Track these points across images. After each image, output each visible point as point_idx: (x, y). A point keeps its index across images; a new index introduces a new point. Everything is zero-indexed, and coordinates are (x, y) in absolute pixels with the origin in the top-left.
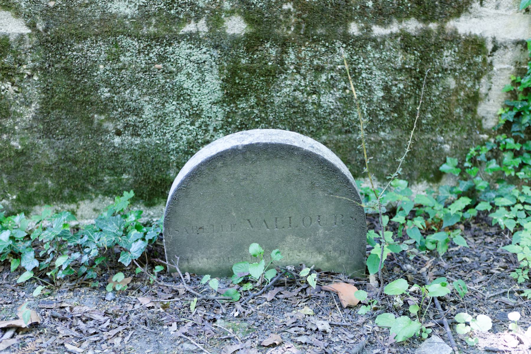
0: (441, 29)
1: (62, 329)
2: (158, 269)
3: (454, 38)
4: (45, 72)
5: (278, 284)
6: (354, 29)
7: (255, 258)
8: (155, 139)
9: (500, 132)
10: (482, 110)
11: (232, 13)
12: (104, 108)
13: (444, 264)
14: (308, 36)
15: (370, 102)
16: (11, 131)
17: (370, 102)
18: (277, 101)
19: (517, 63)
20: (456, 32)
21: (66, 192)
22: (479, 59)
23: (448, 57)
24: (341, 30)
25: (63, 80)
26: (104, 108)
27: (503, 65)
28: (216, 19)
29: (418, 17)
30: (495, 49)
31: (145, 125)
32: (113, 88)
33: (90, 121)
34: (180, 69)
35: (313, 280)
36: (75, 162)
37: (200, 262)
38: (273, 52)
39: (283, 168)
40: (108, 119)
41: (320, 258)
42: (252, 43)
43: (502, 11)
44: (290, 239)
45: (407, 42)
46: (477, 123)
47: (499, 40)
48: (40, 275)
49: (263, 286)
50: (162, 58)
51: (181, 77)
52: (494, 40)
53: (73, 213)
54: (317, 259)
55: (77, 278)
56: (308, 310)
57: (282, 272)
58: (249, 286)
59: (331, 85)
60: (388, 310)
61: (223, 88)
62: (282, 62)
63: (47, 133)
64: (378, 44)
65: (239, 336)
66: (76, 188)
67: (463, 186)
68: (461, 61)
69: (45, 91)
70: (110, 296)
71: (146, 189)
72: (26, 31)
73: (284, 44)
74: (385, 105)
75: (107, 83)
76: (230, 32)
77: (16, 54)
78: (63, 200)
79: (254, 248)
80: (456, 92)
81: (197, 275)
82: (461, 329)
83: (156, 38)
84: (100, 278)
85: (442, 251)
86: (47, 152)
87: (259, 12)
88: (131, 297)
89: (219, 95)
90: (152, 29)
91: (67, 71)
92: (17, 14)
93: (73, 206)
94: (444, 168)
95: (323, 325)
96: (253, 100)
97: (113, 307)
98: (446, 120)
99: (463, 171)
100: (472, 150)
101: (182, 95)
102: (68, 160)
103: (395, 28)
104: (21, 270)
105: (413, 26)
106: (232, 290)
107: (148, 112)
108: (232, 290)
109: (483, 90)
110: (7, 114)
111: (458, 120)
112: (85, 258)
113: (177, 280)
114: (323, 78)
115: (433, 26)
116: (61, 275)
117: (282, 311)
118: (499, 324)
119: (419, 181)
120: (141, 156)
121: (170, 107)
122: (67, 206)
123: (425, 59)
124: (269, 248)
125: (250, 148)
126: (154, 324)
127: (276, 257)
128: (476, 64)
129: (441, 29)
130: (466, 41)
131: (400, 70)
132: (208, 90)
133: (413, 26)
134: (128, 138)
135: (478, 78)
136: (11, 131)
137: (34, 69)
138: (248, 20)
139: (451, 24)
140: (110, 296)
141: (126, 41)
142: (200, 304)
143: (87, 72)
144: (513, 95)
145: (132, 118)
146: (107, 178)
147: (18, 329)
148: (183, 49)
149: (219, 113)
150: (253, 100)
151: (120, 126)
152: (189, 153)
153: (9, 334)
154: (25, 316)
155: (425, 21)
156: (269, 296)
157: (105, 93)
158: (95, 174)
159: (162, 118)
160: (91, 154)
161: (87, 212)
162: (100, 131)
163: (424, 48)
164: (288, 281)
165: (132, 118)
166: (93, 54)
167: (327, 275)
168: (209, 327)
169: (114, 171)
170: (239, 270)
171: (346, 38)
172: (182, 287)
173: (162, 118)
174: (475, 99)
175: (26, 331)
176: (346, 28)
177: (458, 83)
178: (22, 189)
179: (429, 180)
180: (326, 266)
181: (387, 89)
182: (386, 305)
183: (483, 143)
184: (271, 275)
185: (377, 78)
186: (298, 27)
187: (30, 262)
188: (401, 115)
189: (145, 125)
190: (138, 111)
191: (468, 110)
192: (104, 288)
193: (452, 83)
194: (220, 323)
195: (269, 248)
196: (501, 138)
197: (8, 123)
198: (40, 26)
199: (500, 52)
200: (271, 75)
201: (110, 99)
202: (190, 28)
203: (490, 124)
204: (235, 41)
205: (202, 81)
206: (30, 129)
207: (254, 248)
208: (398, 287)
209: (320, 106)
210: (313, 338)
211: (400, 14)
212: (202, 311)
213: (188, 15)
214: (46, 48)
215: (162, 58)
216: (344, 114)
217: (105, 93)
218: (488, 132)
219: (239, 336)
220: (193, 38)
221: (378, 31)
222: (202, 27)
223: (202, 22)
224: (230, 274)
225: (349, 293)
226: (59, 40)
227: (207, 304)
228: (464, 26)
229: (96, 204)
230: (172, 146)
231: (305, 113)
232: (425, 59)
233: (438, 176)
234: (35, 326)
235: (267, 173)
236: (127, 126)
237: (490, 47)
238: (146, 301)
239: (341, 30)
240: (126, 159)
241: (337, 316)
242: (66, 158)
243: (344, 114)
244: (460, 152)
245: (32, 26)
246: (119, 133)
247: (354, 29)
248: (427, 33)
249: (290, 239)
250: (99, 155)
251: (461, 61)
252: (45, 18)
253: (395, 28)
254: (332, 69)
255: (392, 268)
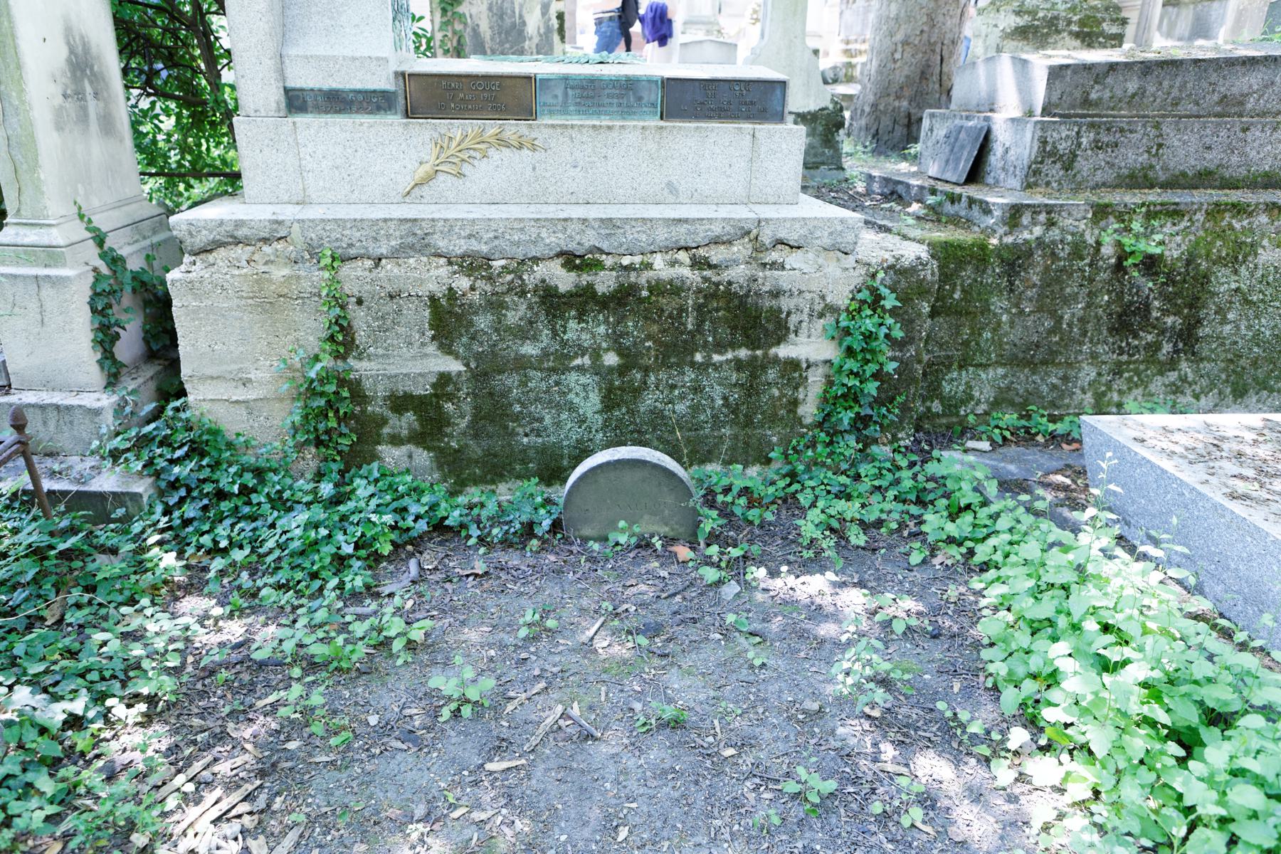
0: (766, 355)
1: (503, 575)
2: (559, 536)
3: (776, 360)
4: (475, 396)
5: (638, 546)
6: (698, 357)
7: (623, 531)
8: (553, 439)
9: (816, 426)
10: (801, 411)
11: (608, 350)
12: (517, 418)
13: (757, 532)
14: (663, 363)
15: (713, 408)
16: (451, 436)
17: (713, 408)
18: (642, 409)
19: (827, 376)
20: (777, 356)
21: (489, 477)
22: (797, 375)
23: (772, 374)
24: (689, 358)
25: (489, 401)
26: (517, 418)
27: (816, 380)
28: (596, 354)
29: (747, 347)
30: (808, 367)
31: (545, 430)
32: (523, 405)
33: (506, 427)
34: (570, 390)
35: (658, 545)
36: (495, 456)
37: (587, 531)
38: (638, 376)
39: (639, 474)
40: (519, 425)
41: (667, 529)
42: (622, 370)
43: (813, 339)
44: (646, 517)
45: (739, 365)
46: (799, 421)
47: (812, 360)
48: (481, 540)
49: (628, 549)
50: (557, 384)
51: (571, 396)
52: (807, 361)
53: (494, 492)
54: (664, 530)
55: (506, 543)
56: (657, 564)
57: (641, 538)
58: (619, 548)
59: (682, 397)
60: (707, 564)
61: (602, 402)
62: (645, 383)
63: (476, 436)
64: (717, 367)
65: (611, 580)
66: (496, 474)
67: (787, 468)
68: (783, 377)
69: (475, 408)
70: (529, 554)
71: (546, 474)
72: (463, 368)
73: (646, 370)
74: (725, 410)
75: (519, 401)
76: (606, 363)
77: (455, 384)
78: (487, 483)
79: (622, 524)
80: (780, 398)
81: (585, 540)
82: (749, 577)
83: (553, 370)
84: (521, 543)
85: (757, 522)
86: (476, 449)
87: (628, 348)
88: (543, 554)
89: (599, 407)
90: (551, 364)
91: (491, 394)
92: (457, 357)
93: (493, 487)
94: (772, 455)
95: (664, 573)
96: (624, 410)
97: (532, 561)
98: (773, 419)
99: (787, 456)
100: (794, 442)
101: (572, 408)
102: (490, 454)
103: (729, 356)
104: (469, 537)
105: (743, 353)
106: (608, 551)
107: (548, 420)
108: (608, 551)
109: (801, 396)
110: (449, 424)
111: (782, 418)
112: (512, 530)
113: (572, 544)
114: (676, 392)
115: (759, 353)
116: (496, 540)
117: (639, 565)
118: (774, 574)
119: (753, 465)
120: (542, 450)
121: (564, 416)
122: (489, 487)
123: (753, 376)
124: (631, 523)
125: (619, 462)
126: (559, 572)
127: (636, 529)
128: (794, 378)
129: (766, 355)
130: (785, 363)
131: (735, 385)
132: (591, 404)
133: (743, 353)
134: (533, 438)
135: (796, 388)
136: (451, 436)
137: (468, 394)
138: (620, 354)
139: (773, 351)
140: (529, 554)
141: (532, 373)
142: (587, 560)
143: (506, 393)
144: (825, 400)
145: (536, 425)
146: (518, 467)
147: (476, 575)
148: (572, 377)
149: (599, 419)
150: (624, 410)
151: (528, 430)
152: (578, 460)
153: (471, 578)
154: (480, 567)
155: (753, 349)
156: (632, 555)
157: (517, 408)
158: (510, 464)
159: (558, 424)
160: (507, 450)
161: (505, 492)
162: (513, 434)
163: (753, 368)
164: (644, 544)
165: (536, 425)
166: (509, 382)
167: (670, 541)
168: (593, 574)
169: (524, 462)
170: (613, 537)
171: (692, 364)
172: (575, 548)
173: (558, 424)
174: (795, 403)
175: (482, 576)
176: (693, 357)
177: (781, 392)
178: (458, 476)
179: (761, 464)
180: (671, 534)
181: (725, 398)
182: (708, 562)
183: (803, 435)
184: (633, 540)
185: (717, 392)
186: (657, 358)
187: (475, 532)
188: (737, 417)
189: (545, 430)
190: (541, 420)
191: (789, 411)
192: (524, 548)
193: (776, 392)
194: (600, 572)
195: (631, 523)
196: (817, 431)
197: (449, 430)
198: (473, 365)
199: (813, 368)
200: (637, 392)
201: (521, 412)
202: (578, 361)
203: (808, 421)
204: (611, 369)
205: (586, 398)
206: (464, 434)
207: (622, 524)
208: (714, 550)
209: (674, 412)
210: (657, 582)
211: (733, 345)
212: (589, 565)
213: (576, 353)
214: (477, 380)
215: (557, 384)
216: (693, 417)
217: (517, 408)
218: (806, 427)
219: (611, 580)
220: (581, 369)
221: (716, 358)
222: (587, 360)
223: (587, 357)
224: (607, 539)
225: (684, 552)
226: (486, 374)
227: (592, 560)
228: (783, 351)
229: (509, 485)
230: (565, 443)
231: (663, 417)
232: (753, 376)
233: (768, 461)
234: (486, 573)
235: (629, 477)
236: (532, 430)
237: (804, 366)
238: (553, 558)
239: (689, 358)
240: (531, 453)
241: (675, 568)
242: (489, 453)
243: (693, 417)
244: (785, 441)
245: (467, 365)
246: (526, 435)
247: (698, 357)
248: (755, 358)
249: (646, 517)
250: (512, 450)
251: (783, 377)
252: (476, 360)
253: (729, 356)
254: (683, 386)
255: (713, 538)
